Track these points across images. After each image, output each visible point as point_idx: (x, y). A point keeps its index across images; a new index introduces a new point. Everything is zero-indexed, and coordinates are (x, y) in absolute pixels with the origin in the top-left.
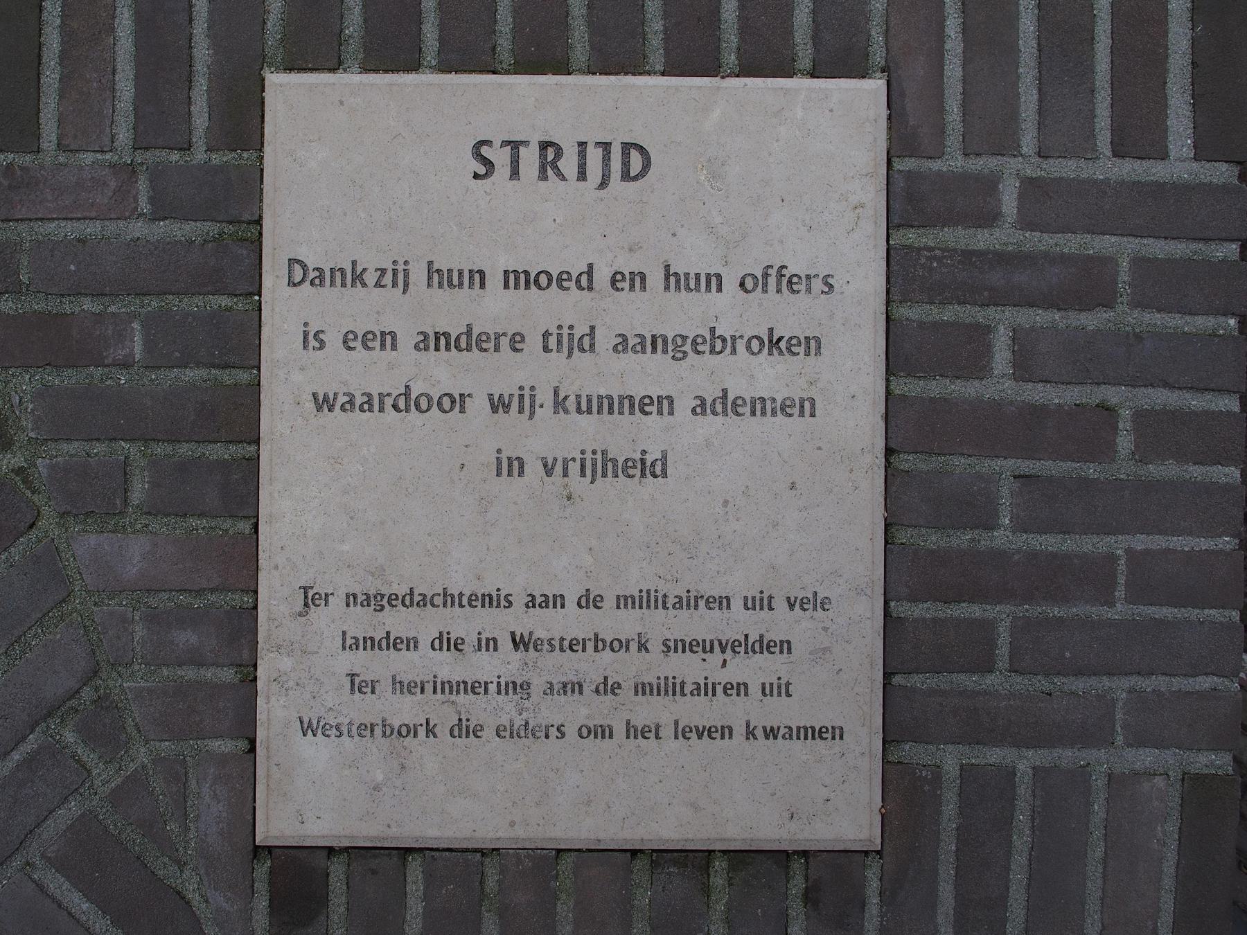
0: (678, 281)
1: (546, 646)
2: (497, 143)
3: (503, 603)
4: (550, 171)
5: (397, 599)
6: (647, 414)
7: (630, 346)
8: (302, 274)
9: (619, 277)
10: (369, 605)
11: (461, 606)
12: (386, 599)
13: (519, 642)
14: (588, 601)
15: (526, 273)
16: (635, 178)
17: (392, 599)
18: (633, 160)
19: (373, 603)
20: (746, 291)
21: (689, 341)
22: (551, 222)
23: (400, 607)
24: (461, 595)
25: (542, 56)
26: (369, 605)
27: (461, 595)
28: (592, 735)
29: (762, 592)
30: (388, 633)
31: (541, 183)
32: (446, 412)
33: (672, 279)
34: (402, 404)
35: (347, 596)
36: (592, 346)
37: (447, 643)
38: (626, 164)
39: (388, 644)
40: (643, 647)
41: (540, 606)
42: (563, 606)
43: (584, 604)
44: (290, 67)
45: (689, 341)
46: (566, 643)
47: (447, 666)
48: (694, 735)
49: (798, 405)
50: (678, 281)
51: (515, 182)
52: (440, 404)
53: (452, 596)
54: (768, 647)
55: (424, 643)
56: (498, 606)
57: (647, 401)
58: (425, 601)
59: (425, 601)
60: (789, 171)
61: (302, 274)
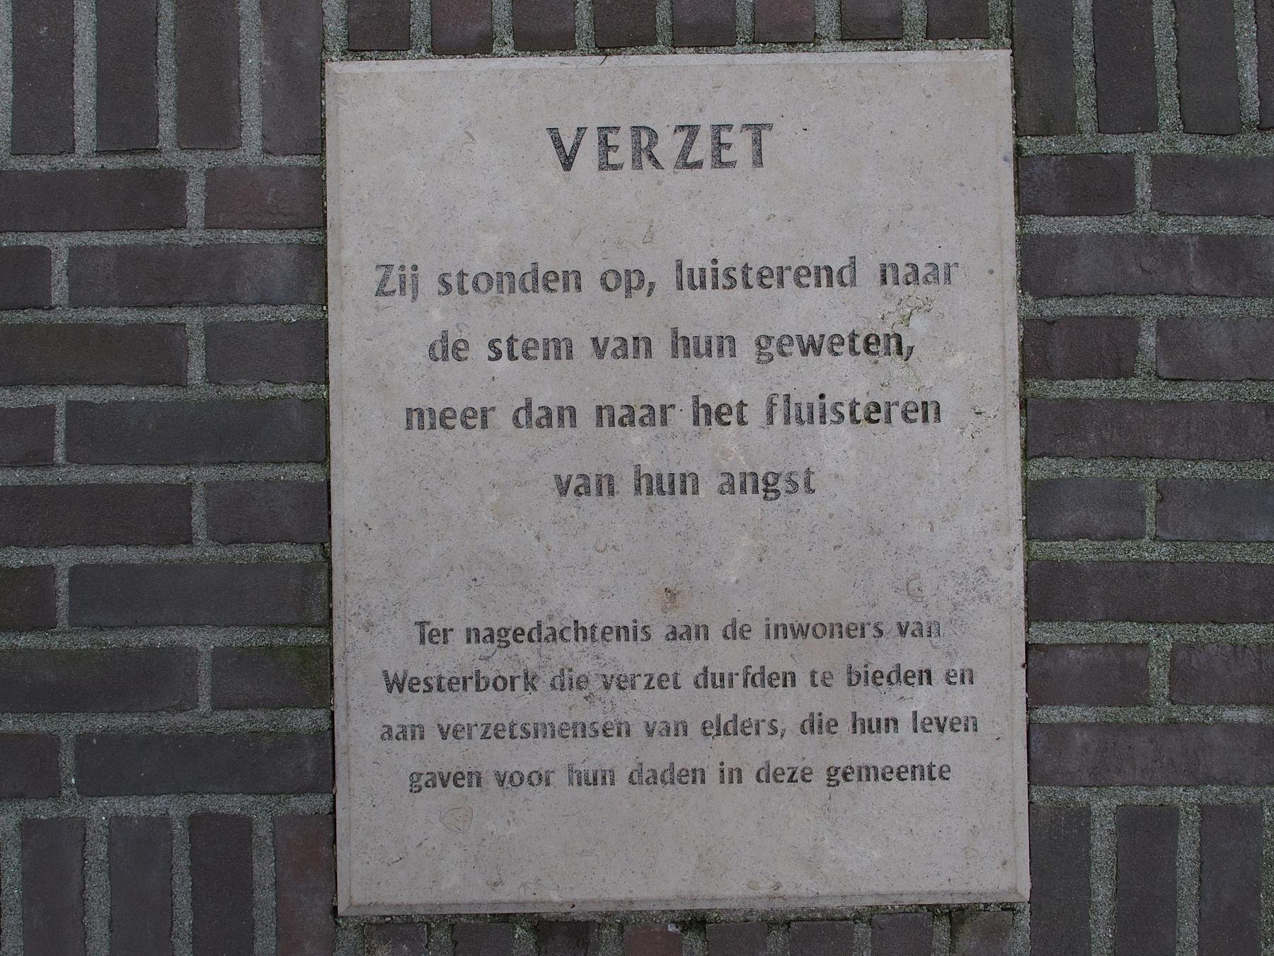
1: (423, 686)
2: (736, 128)
4: (644, 158)
8: (397, 282)
10: (492, 642)
14: (734, 631)
17: (518, 633)
20: (608, 289)
23: (526, 642)
24: (593, 628)
25: (622, 32)
27: (593, 628)
28: (544, 783)
29: (635, 621)
30: (763, 668)
37: (567, 682)
39: (763, 680)
42: (706, 638)
43: (729, 635)
45: (774, 343)
46: (444, 682)
47: (874, 703)
49: (479, 416)
53: (584, 629)
54: (906, 678)
55: (686, 682)
56: (635, 638)
57: (470, 413)
60: (909, 155)
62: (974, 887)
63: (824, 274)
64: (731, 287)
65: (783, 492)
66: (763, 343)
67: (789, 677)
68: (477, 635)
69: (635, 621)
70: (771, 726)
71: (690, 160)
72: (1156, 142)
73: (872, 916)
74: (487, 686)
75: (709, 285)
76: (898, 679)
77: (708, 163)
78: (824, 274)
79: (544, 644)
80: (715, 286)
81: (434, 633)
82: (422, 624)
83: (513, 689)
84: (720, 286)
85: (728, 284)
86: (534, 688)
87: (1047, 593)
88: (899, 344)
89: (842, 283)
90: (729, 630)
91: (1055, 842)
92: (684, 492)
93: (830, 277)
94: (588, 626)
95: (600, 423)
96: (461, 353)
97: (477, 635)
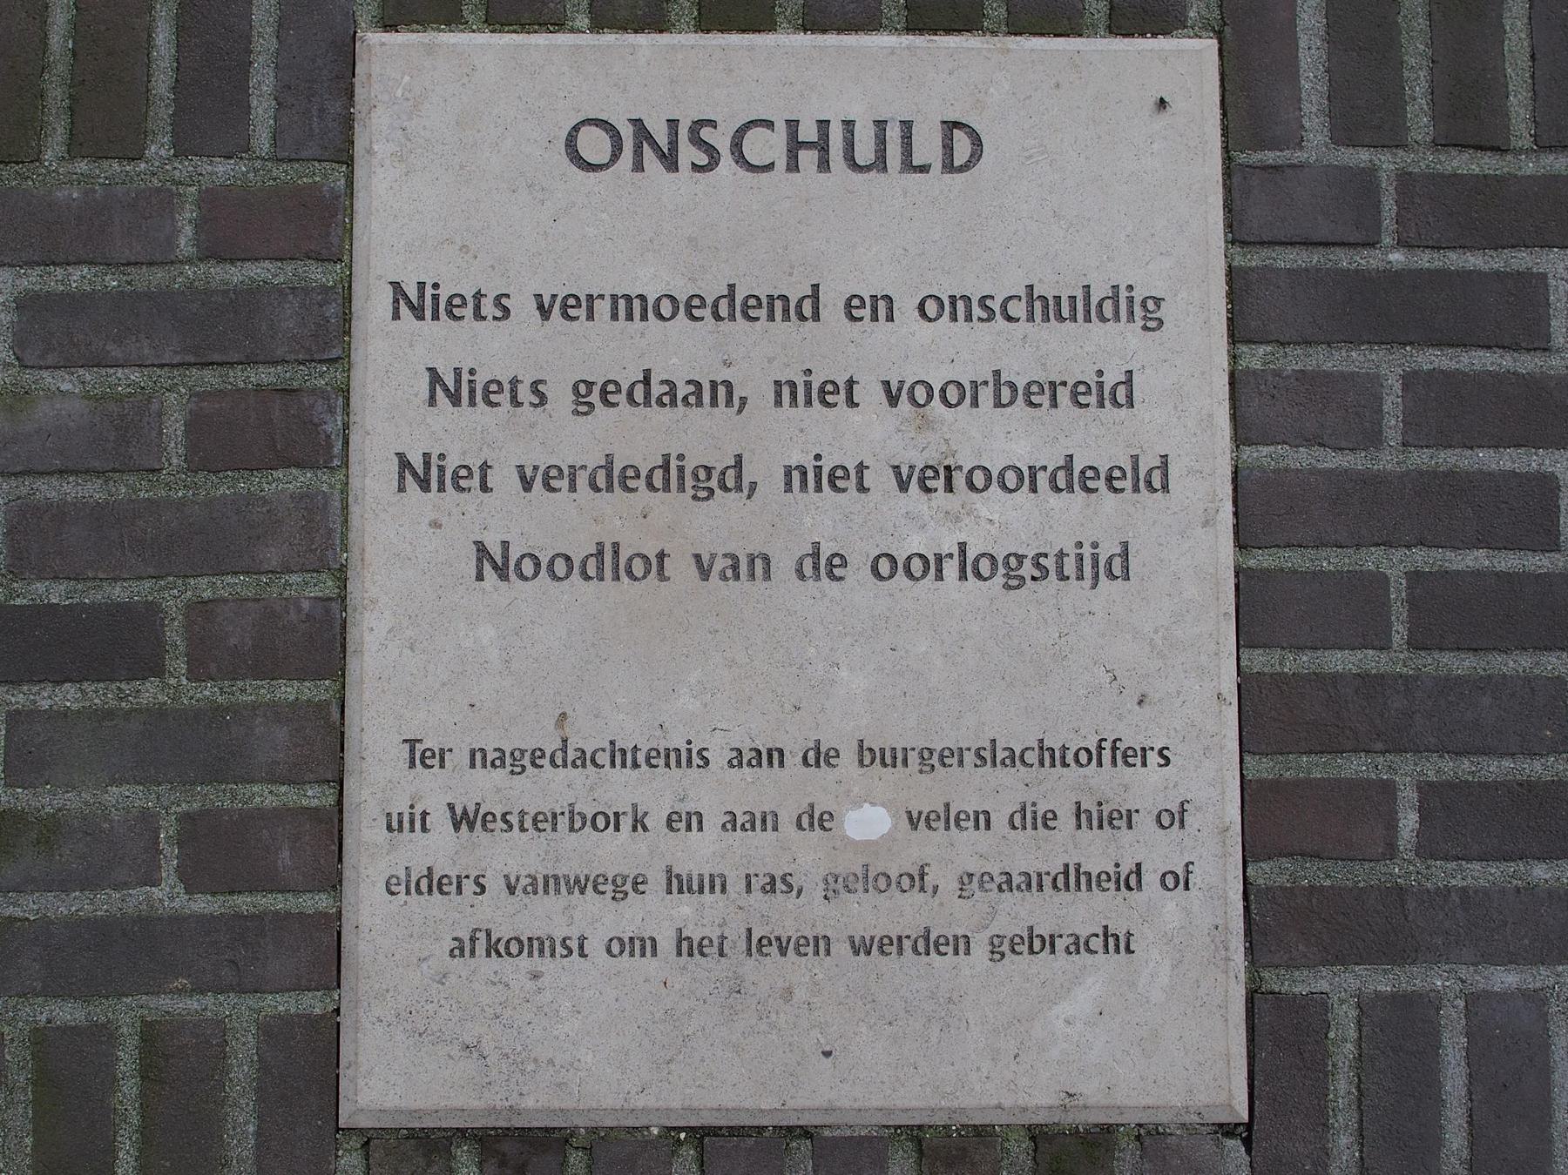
0: (1046, 307)
3: (696, 760)
5: (543, 756)
6: (554, 490)
7: (680, 396)
8: (415, 303)
9: (856, 302)
10: (503, 765)
11: (636, 765)
12: (936, 756)
13: (462, 820)
15: (642, 298)
16: (963, 169)
18: (962, 145)
19: (508, 760)
21: (596, 389)
22: (645, 230)
24: (1064, 748)
26: (503, 765)
31: (791, 175)
32: (1011, 491)
33: (1038, 305)
34: (601, 481)
35: (473, 753)
36: (1130, 397)
38: (948, 148)
40: (639, 823)
41: (1003, 763)
44: (389, 26)
45: (596, 389)
48: (774, 950)
50: (1046, 307)
51: (795, 175)
52: (989, 478)
53: (624, 752)
58: (1014, 759)
59: (1014, 759)
60: (1117, 157)
61: (415, 303)
62: (966, 1101)
63: (778, 304)
64: (988, 320)
65: (1028, 579)
66: (583, 389)
67: (982, 817)
68: (484, 758)
69: (689, 742)
70: (478, 884)
71: (956, 164)
72: (1404, 158)
73: (916, 1136)
74: (584, 824)
75: (1080, 316)
76: (811, 824)
77: (937, 166)
78: (778, 304)
79: (746, 769)
80: (969, 318)
81: (428, 754)
82: (412, 743)
83: (617, 829)
84: (975, 318)
85: (984, 315)
86: (645, 829)
87: (1264, 714)
88: (730, 394)
89: (802, 318)
90: (811, 754)
91: (1279, 1034)
92: (752, 576)
93: (786, 310)
94: (1057, 746)
95: (788, 487)
96: (492, 397)
97: (484, 758)
